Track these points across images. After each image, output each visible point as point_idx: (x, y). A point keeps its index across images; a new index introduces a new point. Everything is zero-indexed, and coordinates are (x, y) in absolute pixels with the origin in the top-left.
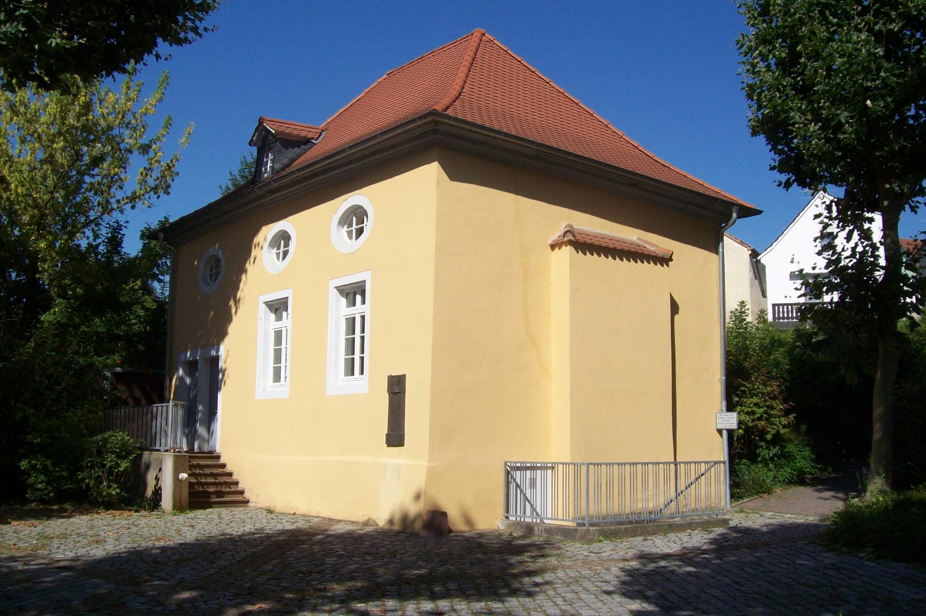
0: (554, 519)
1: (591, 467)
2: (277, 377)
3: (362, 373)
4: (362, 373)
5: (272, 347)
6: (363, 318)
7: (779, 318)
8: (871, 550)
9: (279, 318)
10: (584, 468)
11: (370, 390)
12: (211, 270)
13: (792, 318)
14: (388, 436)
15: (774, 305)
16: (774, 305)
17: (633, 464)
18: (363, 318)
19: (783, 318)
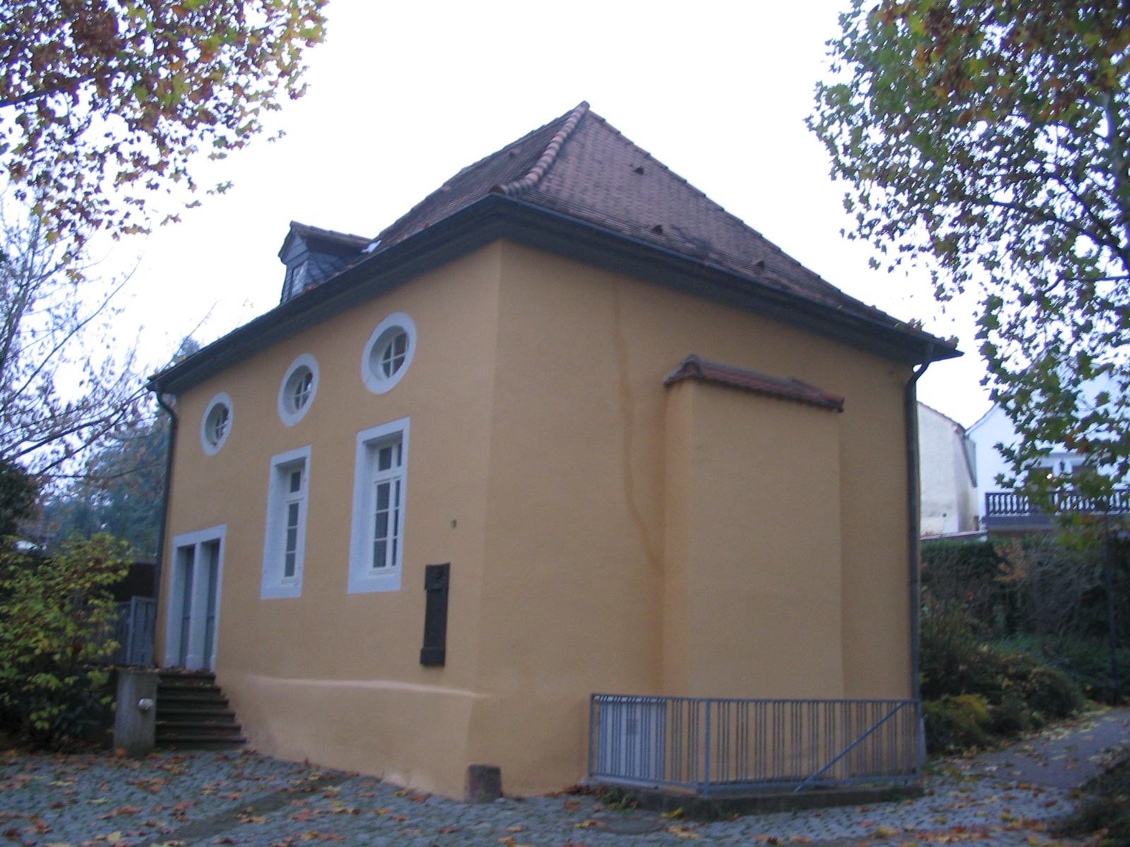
0: (614, 776)
1: (714, 706)
2: (380, 560)
3: (394, 563)
4: (394, 563)
5: (373, 510)
6: (398, 483)
7: (994, 511)
8: (1105, 831)
9: (385, 464)
10: (703, 706)
11: (397, 583)
12: (387, 356)
13: (1024, 511)
14: (423, 653)
15: (988, 495)
16: (988, 495)
17: (779, 702)
18: (398, 483)
19: (1115, 509)
